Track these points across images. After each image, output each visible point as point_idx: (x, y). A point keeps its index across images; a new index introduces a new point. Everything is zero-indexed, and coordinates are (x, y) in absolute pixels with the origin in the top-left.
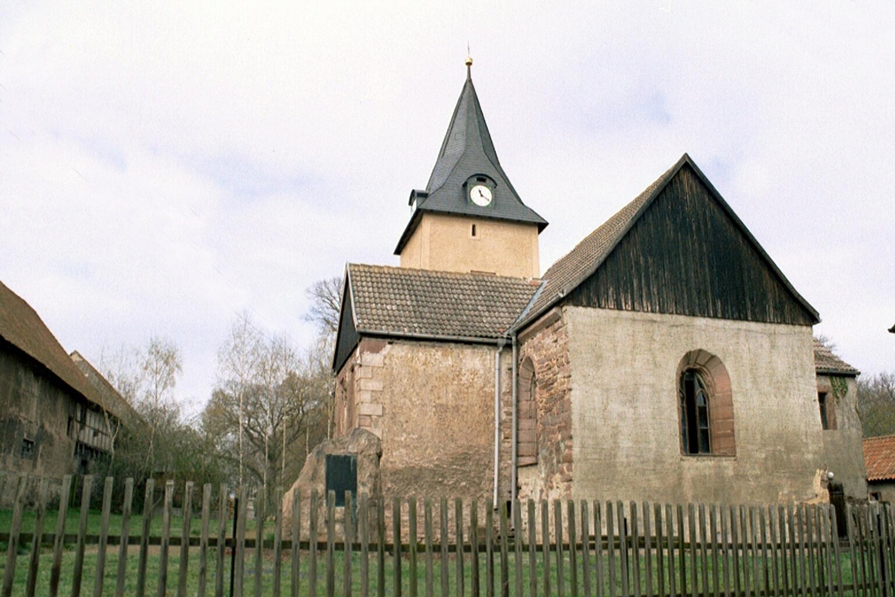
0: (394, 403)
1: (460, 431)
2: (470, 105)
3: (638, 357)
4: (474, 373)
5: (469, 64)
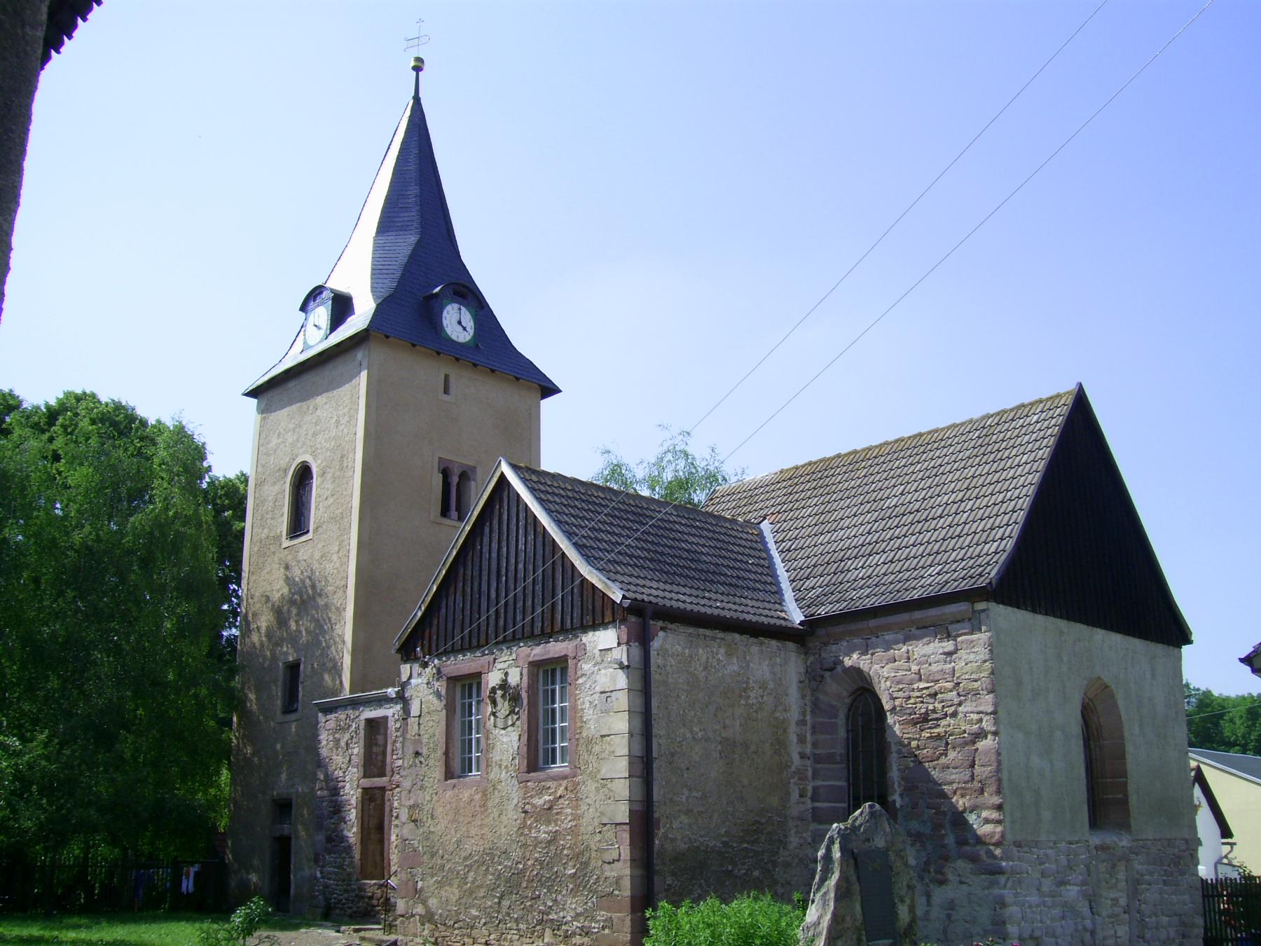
4: (763, 686)
5: (418, 69)
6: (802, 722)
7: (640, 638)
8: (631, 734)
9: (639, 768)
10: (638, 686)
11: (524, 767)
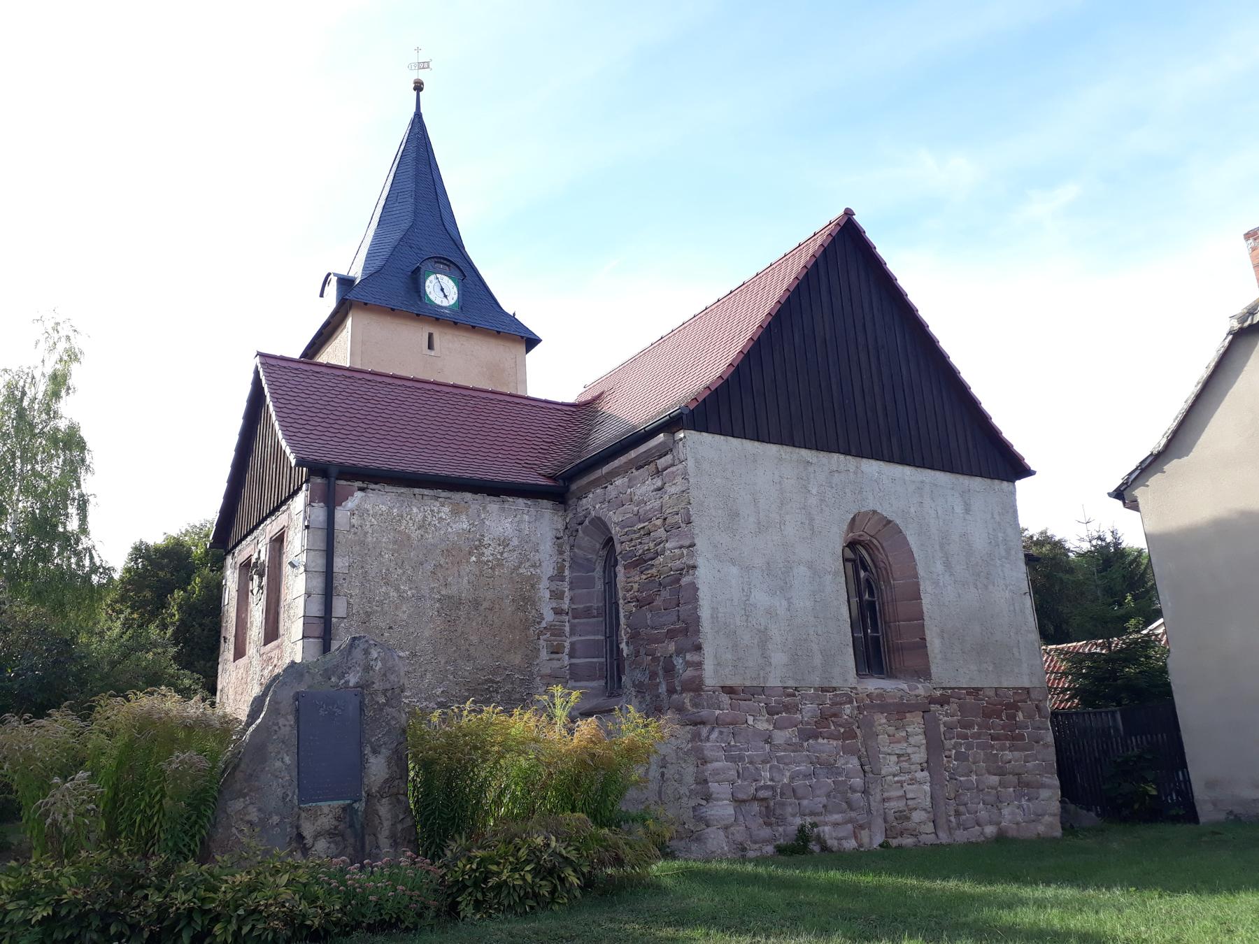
1: (481, 641)
3: (787, 517)
4: (504, 543)
5: (419, 87)
6: (559, 576)
7: (330, 500)
8: (308, 594)
9: (318, 630)
10: (322, 546)
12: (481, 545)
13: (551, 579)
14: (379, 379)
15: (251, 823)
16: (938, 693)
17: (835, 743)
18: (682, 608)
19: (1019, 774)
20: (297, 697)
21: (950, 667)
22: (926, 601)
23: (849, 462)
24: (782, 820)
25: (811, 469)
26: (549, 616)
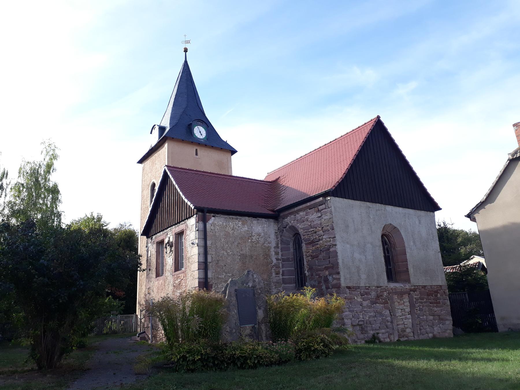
0: (218, 254)
2: (186, 79)
4: (259, 235)
5: (186, 50)
6: (277, 247)
7: (203, 220)
8: (199, 254)
9: (203, 267)
10: (202, 237)
11: (173, 268)
12: (252, 236)
13: (275, 247)
14: (213, 175)
15: (227, 332)
16: (413, 287)
17: (381, 305)
18: (331, 259)
19: (439, 316)
20: (236, 290)
21: (417, 279)
22: (408, 255)
23: (382, 207)
24: (366, 332)
25: (370, 209)
26: (275, 261)
